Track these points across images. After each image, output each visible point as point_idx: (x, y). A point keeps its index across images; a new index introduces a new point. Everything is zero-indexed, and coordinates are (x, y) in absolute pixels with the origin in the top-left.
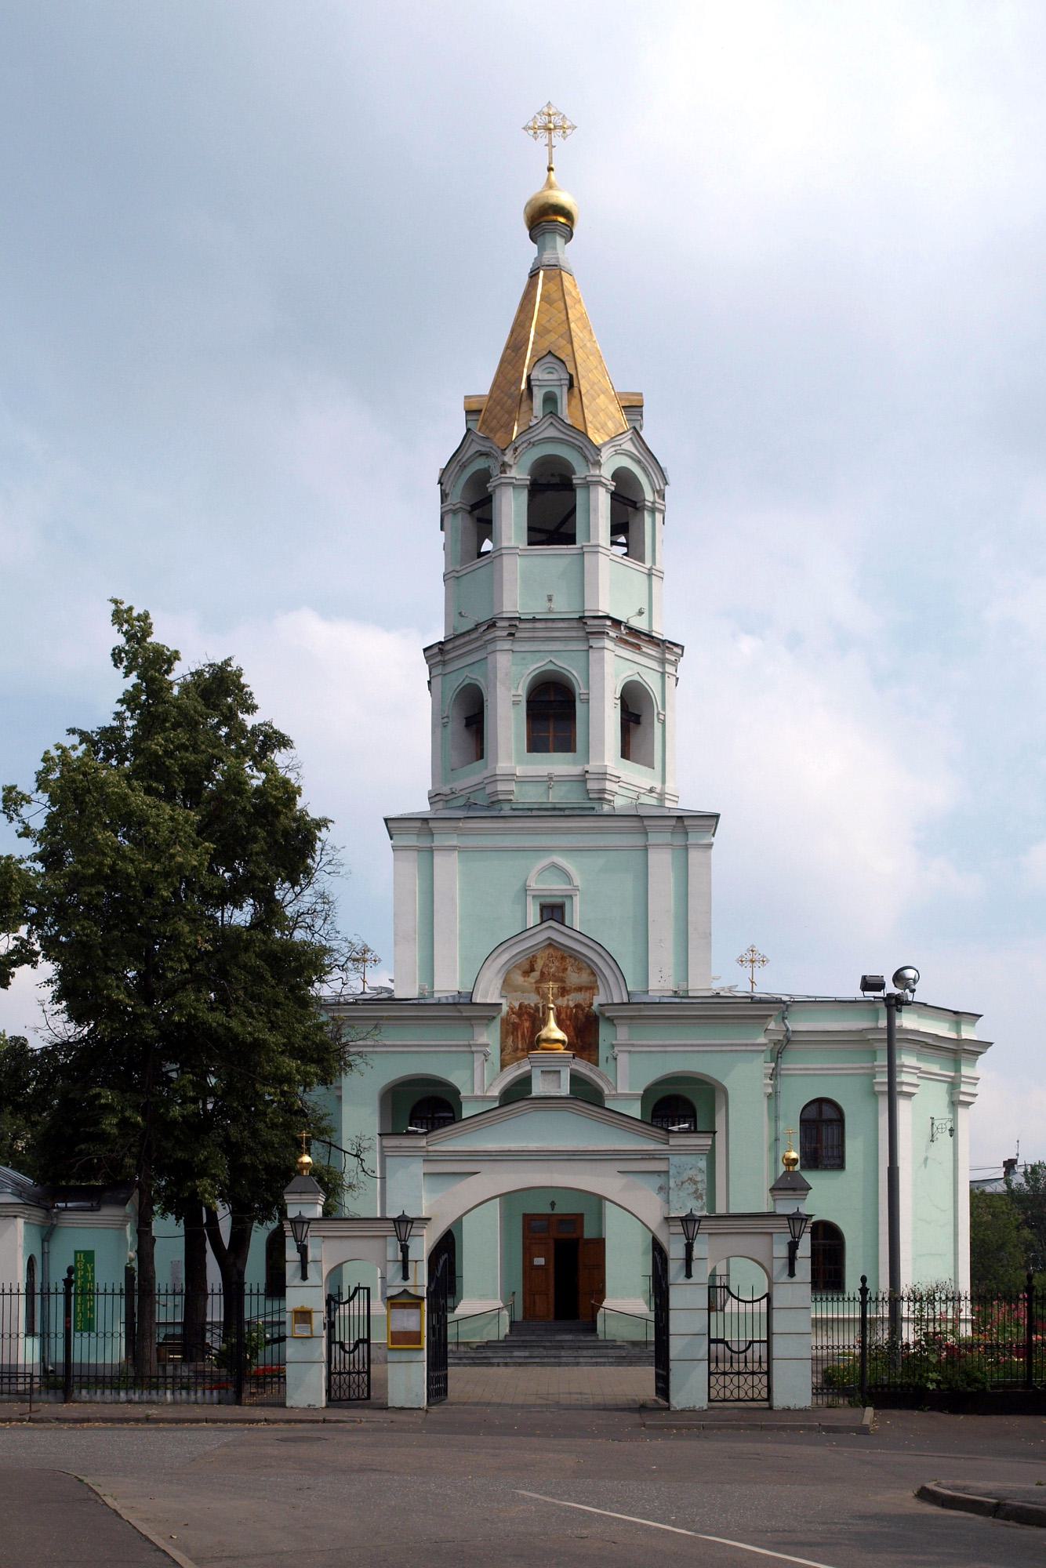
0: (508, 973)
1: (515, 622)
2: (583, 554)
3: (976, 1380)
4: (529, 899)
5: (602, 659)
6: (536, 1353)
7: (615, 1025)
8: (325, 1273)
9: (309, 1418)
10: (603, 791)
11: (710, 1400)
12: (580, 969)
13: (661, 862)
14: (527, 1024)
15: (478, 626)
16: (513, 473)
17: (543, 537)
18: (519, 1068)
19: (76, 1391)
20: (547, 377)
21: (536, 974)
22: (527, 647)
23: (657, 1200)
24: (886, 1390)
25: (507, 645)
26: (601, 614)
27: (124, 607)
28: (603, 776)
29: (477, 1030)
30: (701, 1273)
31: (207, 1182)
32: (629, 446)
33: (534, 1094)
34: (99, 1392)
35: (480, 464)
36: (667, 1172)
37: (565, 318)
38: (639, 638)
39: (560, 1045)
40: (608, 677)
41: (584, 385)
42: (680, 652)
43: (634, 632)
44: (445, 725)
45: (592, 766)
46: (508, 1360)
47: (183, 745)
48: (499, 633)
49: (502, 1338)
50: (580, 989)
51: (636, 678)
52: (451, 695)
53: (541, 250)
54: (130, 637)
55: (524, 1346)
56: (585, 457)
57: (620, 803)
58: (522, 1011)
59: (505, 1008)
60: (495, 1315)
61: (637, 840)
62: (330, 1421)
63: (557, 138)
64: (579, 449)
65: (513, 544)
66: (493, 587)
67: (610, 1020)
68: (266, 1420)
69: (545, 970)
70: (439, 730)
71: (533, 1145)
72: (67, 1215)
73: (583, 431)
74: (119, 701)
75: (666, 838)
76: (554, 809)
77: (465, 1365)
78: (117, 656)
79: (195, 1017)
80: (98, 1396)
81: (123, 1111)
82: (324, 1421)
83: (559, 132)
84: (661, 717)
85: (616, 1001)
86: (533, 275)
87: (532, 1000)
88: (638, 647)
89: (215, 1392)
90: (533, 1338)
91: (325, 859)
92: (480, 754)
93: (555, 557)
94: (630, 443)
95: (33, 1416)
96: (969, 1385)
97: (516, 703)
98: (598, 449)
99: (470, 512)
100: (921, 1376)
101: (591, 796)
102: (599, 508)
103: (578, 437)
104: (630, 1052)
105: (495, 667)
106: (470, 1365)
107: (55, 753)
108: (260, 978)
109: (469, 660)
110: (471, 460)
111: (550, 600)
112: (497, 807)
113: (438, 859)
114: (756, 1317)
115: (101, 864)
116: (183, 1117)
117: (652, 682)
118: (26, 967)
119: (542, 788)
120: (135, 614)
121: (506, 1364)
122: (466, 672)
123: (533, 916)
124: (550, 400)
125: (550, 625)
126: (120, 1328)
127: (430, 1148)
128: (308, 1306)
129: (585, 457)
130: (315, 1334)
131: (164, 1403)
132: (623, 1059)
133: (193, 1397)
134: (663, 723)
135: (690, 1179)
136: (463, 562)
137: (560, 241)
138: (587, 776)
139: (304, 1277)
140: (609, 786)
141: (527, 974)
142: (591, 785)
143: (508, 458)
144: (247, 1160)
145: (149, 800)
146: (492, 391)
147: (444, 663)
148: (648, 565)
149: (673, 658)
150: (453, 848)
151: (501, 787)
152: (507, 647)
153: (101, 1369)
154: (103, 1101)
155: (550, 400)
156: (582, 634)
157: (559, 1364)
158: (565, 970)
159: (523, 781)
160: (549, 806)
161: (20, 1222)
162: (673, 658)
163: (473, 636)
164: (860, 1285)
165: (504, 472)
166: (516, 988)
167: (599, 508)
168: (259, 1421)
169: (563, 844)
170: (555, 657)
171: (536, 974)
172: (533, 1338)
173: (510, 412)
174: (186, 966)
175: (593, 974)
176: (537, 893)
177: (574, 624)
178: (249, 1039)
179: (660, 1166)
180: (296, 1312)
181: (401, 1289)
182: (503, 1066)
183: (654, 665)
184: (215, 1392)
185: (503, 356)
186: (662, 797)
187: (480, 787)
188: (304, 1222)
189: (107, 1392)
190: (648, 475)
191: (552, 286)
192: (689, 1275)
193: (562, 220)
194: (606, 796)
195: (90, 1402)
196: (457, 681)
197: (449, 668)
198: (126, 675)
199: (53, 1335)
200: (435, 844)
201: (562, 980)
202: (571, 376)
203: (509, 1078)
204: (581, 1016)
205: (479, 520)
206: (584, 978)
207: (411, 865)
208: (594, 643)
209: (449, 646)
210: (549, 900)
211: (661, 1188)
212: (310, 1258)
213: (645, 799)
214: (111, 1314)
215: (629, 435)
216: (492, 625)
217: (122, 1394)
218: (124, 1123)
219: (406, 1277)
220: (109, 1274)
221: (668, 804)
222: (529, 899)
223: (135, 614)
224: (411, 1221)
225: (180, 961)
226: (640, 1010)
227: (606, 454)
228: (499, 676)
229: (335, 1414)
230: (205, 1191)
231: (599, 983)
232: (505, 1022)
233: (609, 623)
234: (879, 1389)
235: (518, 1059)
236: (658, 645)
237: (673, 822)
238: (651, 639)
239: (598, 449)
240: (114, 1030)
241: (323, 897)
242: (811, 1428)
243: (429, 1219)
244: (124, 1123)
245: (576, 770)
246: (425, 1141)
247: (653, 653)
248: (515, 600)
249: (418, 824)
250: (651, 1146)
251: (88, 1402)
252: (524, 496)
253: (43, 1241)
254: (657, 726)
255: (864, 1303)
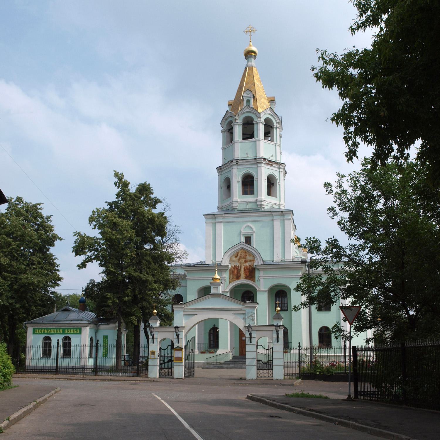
0: (231, 257)
1: (237, 161)
2: (256, 141)
3: (330, 372)
4: (242, 235)
5: (261, 169)
6: (236, 365)
7: (259, 271)
8: (159, 341)
9: (153, 381)
10: (262, 205)
11: (257, 377)
12: (250, 255)
13: (277, 224)
14: (236, 271)
15: (228, 162)
16: (238, 121)
17: (249, 136)
18: (234, 283)
19: (98, 373)
20: (247, 95)
21: (239, 257)
22: (241, 167)
23: (243, 321)
24: (306, 374)
25: (236, 167)
26: (261, 157)
27: (117, 172)
28: (261, 201)
29: (222, 273)
30: (254, 341)
31: (134, 317)
32: (269, 112)
33: (211, 293)
34: (104, 373)
35: (230, 119)
36: (245, 314)
37: (253, 79)
38: (272, 163)
39: (218, 280)
40: (262, 174)
41: (257, 97)
42: (284, 165)
43: (270, 161)
44: (221, 188)
45: (259, 198)
46: (228, 367)
47: (131, 205)
48: (234, 164)
49: (229, 360)
50: (250, 261)
51: (272, 173)
52: (223, 180)
53: (248, 62)
54: (119, 179)
55: (234, 363)
56: (257, 116)
57: (267, 207)
58: (235, 268)
59: (230, 267)
60: (227, 354)
61: (271, 218)
62: (155, 381)
63: (252, 33)
64: (255, 114)
65: (238, 140)
66: (233, 151)
67: (258, 269)
68: (139, 381)
69: (241, 256)
70: (220, 189)
71: (211, 307)
72: (101, 326)
73: (256, 109)
74: (116, 195)
75: (278, 217)
76: (249, 210)
77: (216, 368)
78: (115, 184)
79: (131, 274)
80: (104, 374)
81: (113, 298)
82: (153, 381)
83: (253, 32)
84: (279, 183)
85: (260, 264)
86: (246, 69)
87: (237, 264)
88: (272, 165)
89: (132, 373)
90: (237, 361)
91: (176, 229)
92: (230, 196)
93: (249, 143)
94: (269, 111)
95: (84, 378)
96: (328, 373)
97: (238, 182)
98: (260, 114)
99: (228, 131)
100: (315, 371)
101: (258, 206)
102: (260, 129)
103: (255, 111)
104: (264, 278)
105: (233, 173)
106: (218, 368)
107: (96, 210)
108: (150, 263)
109: (227, 171)
110: (228, 118)
111: (247, 154)
112: (234, 210)
113: (218, 225)
114: (296, 354)
115: (107, 236)
116: (128, 300)
117: (276, 174)
118: (90, 263)
119: (245, 205)
120: (119, 173)
121: (227, 368)
122: (226, 174)
123: (243, 240)
124: (248, 101)
125: (247, 161)
126: (114, 356)
127: (185, 308)
128: (154, 350)
129: (257, 116)
130: (156, 358)
131: (119, 376)
132: (262, 280)
133: (126, 375)
134: (280, 185)
135: (251, 316)
136: (226, 144)
137: (253, 59)
138: (257, 201)
139: (153, 343)
140: (263, 203)
141: (236, 257)
142: (258, 203)
143: (236, 117)
144: (147, 311)
145: (120, 220)
146: (235, 99)
147: (221, 172)
148: (275, 142)
149: (282, 167)
150: (221, 222)
151: (234, 205)
152: (236, 167)
153: (108, 367)
154: (108, 296)
155: (248, 101)
156: (256, 163)
157: (241, 368)
158: (246, 256)
159: (241, 203)
160: (247, 209)
161: (88, 328)
162: (282, 167)
163: (228, 164)
164: (298, 345)
165: (235, 121)
166: (233, 261)
167: (260, 129)
168: (137, 381)
169: (251, 220)
170: (249, 169)
171: (239, 257)
172: (237, 361)
173: (238, 105)
174: (129, 261)
175: (254, 256)
176: (243, 234)
177: (254, 160)
178: (144, 279)
179: (243, 312)
180: (151, 352)
181: (177, 346)
182: (230, 283)
183: (277, 169)
184: (132, 373)
185: (238, 90)
186: (279, 205)
187: (229, 205)
188: (152, 328)
189: (106, 373)
190: (275, 119)
191: (250, 71)
192: (251, 342)
193: (253, 54)
194: (263, 206)
195: (102, 375)
196: (224, 177)
197: (223, 173)
198: (118, 188)
199: (82, 358)
200: (217, 221)
201: (245, 258)
202: (253, 95)
203: (231, 286)
204: (250, 269)
205: (82, 302)
206: (251, 258)
207: (210, 228)
208: (259, 165)
209: (222, 167)
210: (247, 236)
211: (244, 318)
212: (155, 337)
213: (274, 206)
214: (112, 352)
215: (269, 109)
216: (232, 162)
217: (109, 374)
218: (114, 302)
219: (178, 343)
220: (112, 341)
221: (281, 207)
222: (242, 235)
223: (119, 173)
224: (179, 327)
225: (128, 260)
226: (266, 266)
227: (262, 115)
228: (234, 175)
229: (161, 379)
230: (133, 319)
231: (255, 259)
232: (230, 270)
233: (263, 159)
234: (306, 374)
235: (234, 281)
236: (278, 164)
237: (280, 213)
238: (276, 163)
239: (260, 114)
240: (111, 278)
241: (175, 239)
242: (278, 384)
243: (184, 327)
244: (114, 302)
245: (254, 199)
246: (184, 306)
247: (276, 166)
248: (239, 154)
249: (212, 216)
250: (241, 307)
251: (102, 375)
252: (241, 127)
253: (96, 333)
254: (278, 186)
255: (299, 350)
